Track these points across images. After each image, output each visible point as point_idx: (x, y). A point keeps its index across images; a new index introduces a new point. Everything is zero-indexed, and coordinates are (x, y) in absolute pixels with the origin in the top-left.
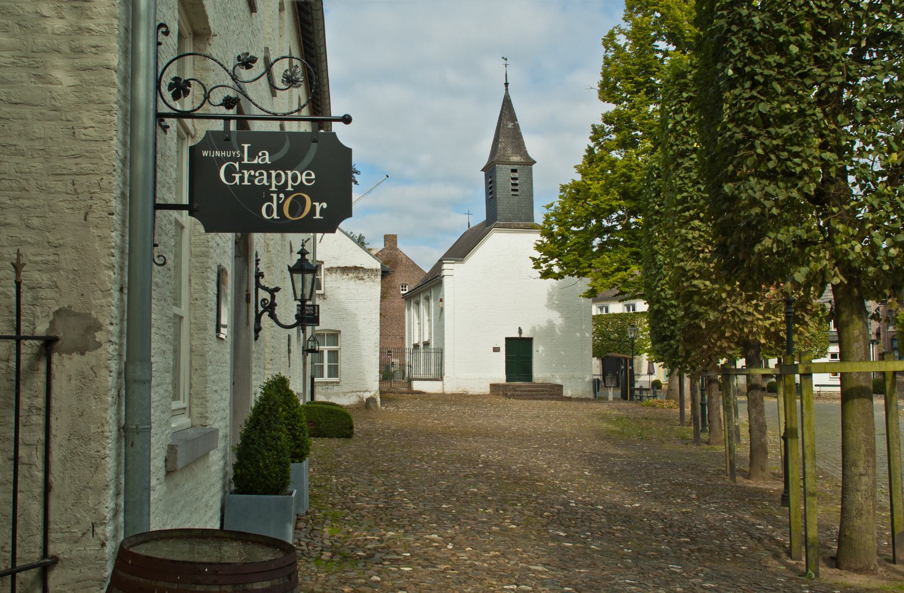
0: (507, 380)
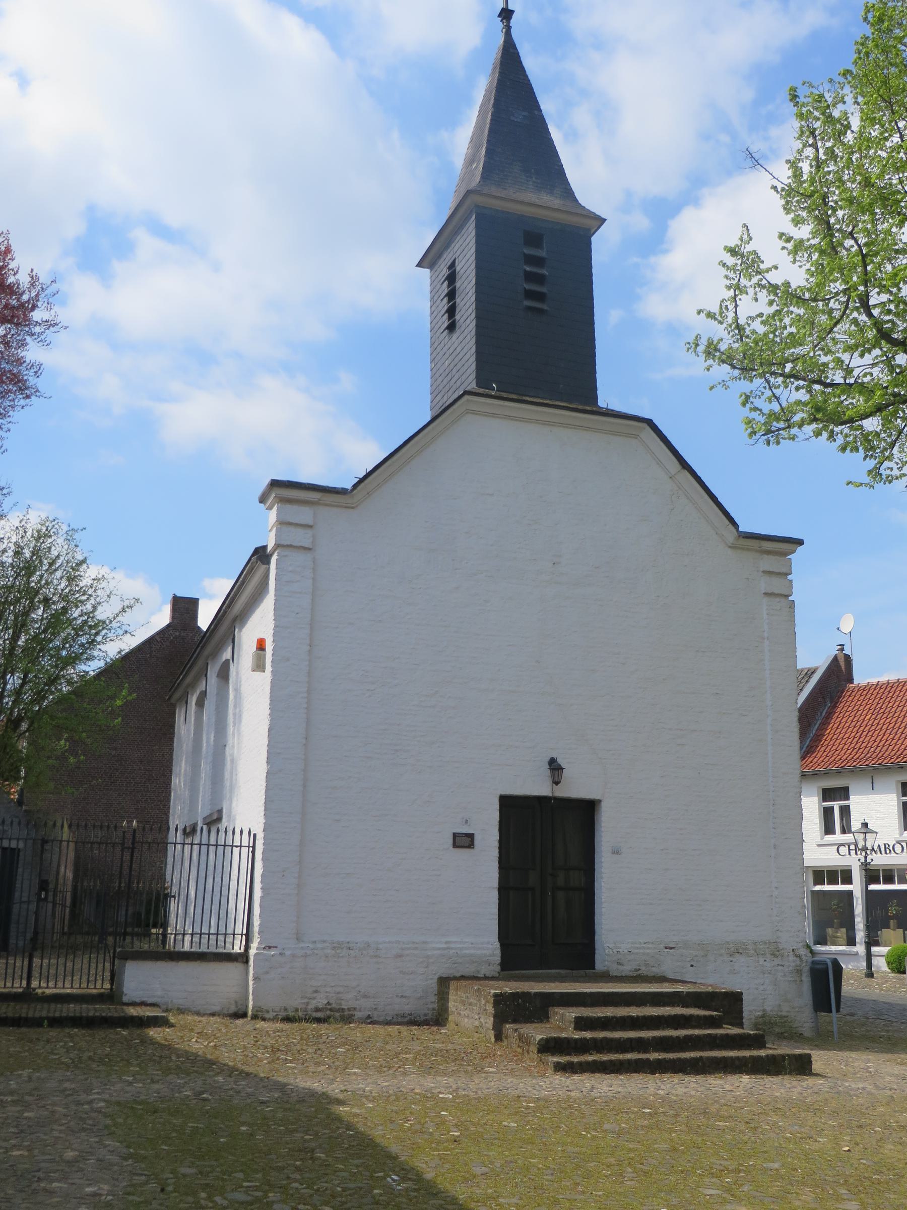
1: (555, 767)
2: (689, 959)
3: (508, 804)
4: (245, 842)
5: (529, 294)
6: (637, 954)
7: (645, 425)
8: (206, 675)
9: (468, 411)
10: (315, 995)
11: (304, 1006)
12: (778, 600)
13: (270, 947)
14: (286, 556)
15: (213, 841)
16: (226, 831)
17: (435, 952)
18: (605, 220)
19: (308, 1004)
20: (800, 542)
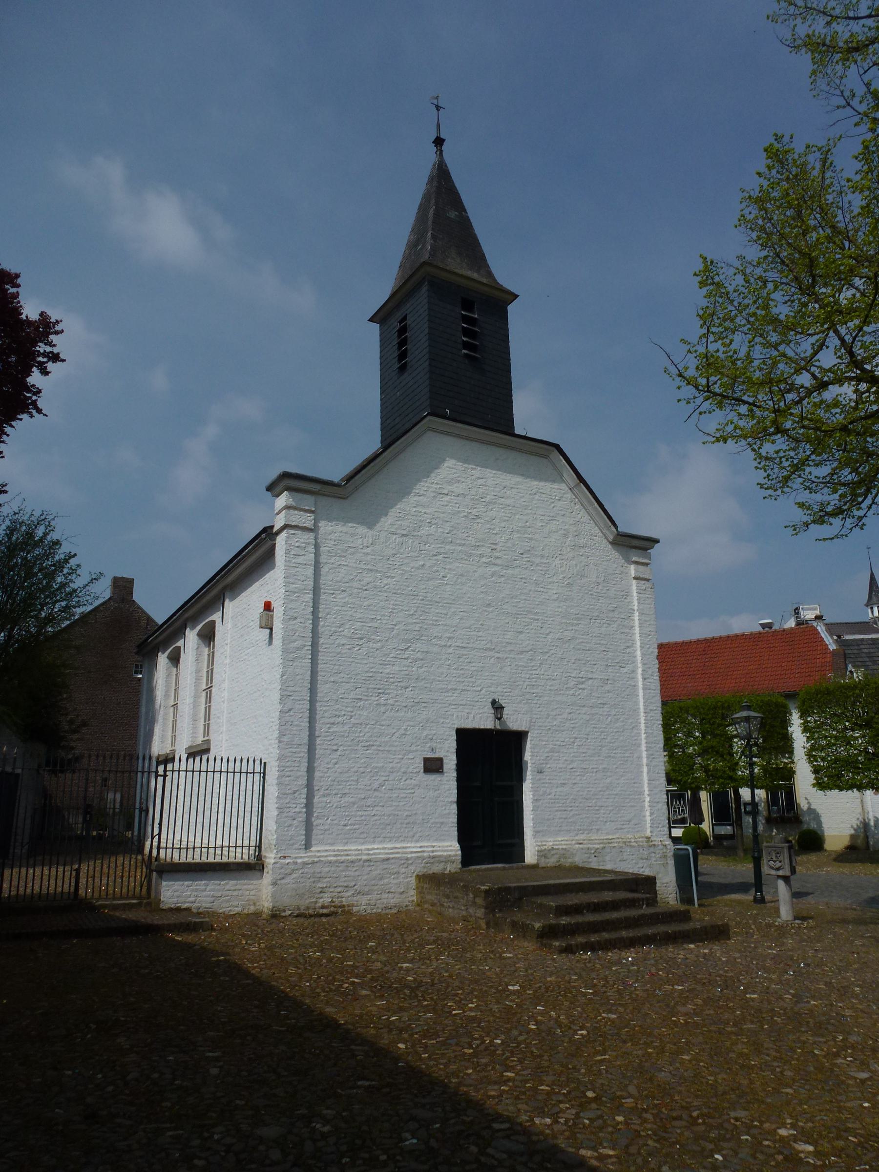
0: (468, 859)
1: (497, 708)
2: (593, 851)
3: (462, 734)
4: (257, 770)
5: (466, 345)
6: (558, 849)
7: (553, 449)
8: (185, 634)
9: (429, 429)
10: (322, 895)
11: (313, 905)
12: (643, 582)
13: (285, 857)
14: (294, 534)
15: (204, 768)
16: (144, 759)
17: (413, 855)
18: (518, 296)
19: (316, 902)
20: (657, 541)
